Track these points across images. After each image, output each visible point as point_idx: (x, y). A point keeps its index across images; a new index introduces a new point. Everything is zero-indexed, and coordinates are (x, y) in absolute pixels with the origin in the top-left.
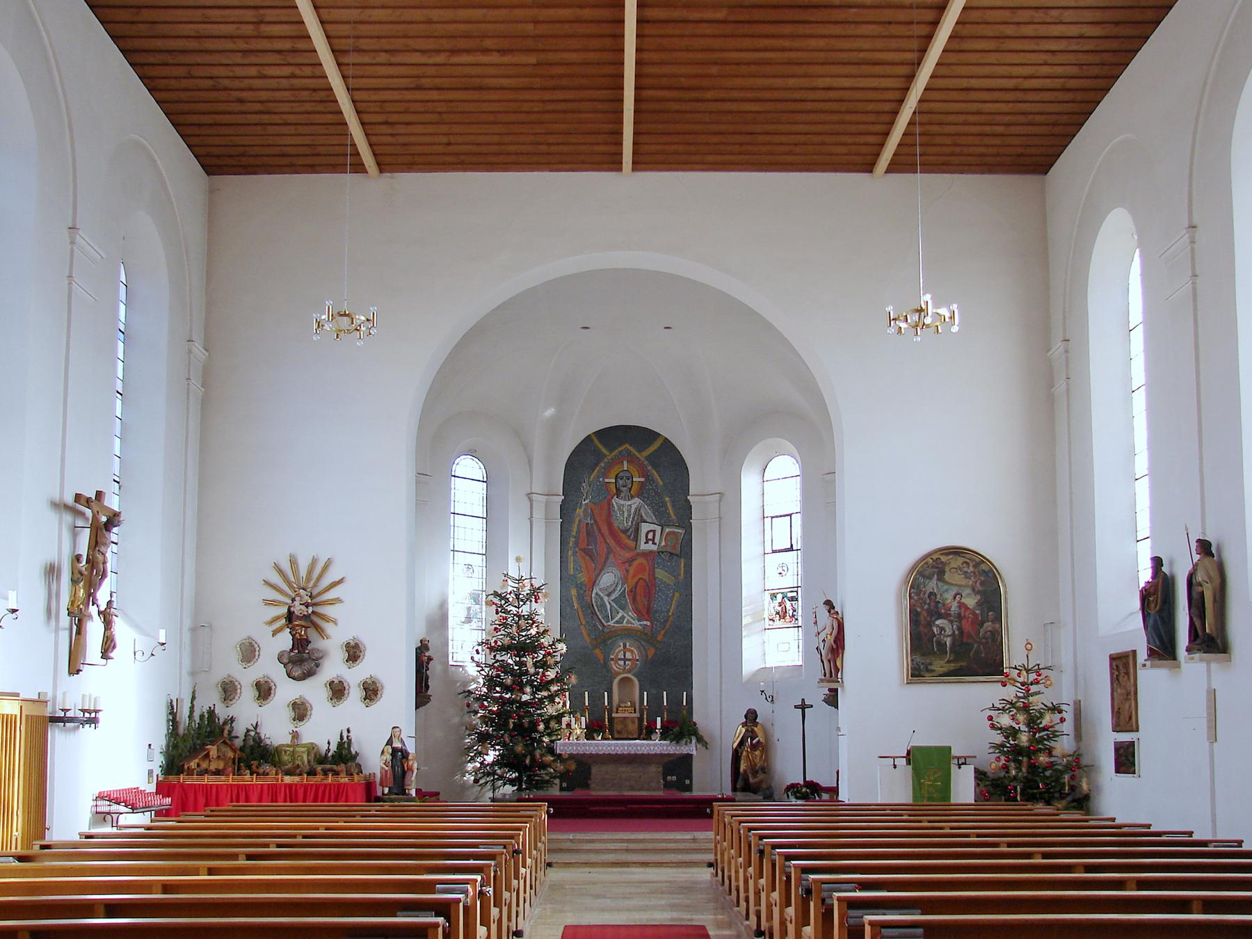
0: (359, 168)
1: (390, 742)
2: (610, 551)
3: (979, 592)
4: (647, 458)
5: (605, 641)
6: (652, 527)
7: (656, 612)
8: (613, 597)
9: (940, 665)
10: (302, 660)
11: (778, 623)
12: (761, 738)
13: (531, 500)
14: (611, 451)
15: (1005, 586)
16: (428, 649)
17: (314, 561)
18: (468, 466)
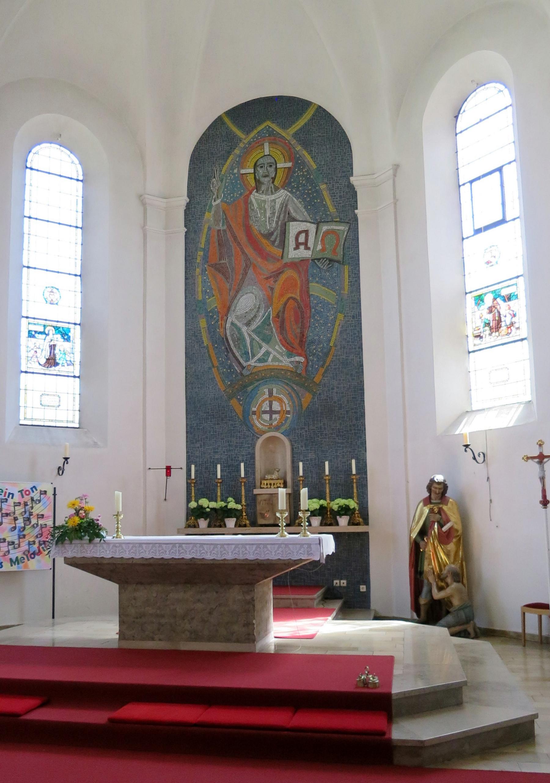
2: (248, 264)
4: (296, 135)
6: (304, 226)
7: (312, 342)
8: (254, 326)
11: (489, 339)
12: (454, 521)
14: (248, 133)
18: (51, 158)
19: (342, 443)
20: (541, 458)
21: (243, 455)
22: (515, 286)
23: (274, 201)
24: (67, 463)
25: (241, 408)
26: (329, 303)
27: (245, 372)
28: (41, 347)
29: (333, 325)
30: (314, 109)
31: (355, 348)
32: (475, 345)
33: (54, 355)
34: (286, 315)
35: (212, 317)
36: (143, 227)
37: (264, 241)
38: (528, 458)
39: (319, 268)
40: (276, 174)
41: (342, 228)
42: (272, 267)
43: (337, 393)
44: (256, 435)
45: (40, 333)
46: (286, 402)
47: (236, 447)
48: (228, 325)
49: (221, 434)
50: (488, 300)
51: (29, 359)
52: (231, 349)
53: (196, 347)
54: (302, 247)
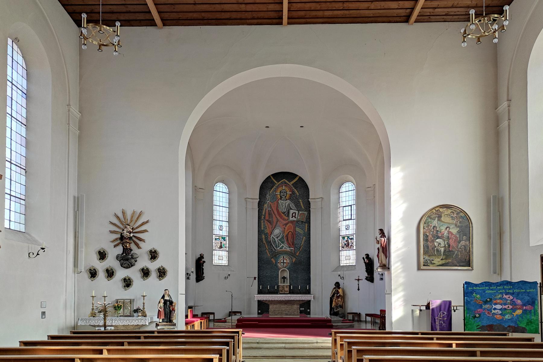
0: (151, 23)
1: (163, 297)
2: (278, 221)
3: (458, 227)
4: (293, 184)
5: (275, 256)
9: (437, 261)
10: (127, 259)
13: (246, 201)
15: (472, 223)
16: (203, 258)
17: (134, 212)
20: (358, 280)
41: (306, 213)
42: (285, 222)
50: (346, 238)
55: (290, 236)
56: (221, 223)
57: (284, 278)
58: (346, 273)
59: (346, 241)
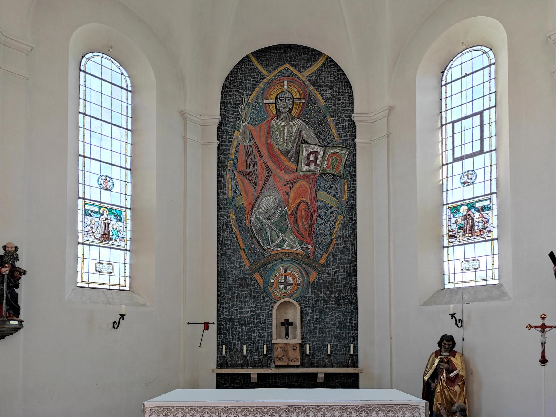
2: (269, 173)
4: (309, 78)
7: (318, 235)
8: (274, 220)
14: (270, 72)
19: (340, 308)
20: (543, 328)
21: (263, 315)
22: (489, 201)
23: (291, 127)
24: (123, 319)
25: (262, 280)
26: (332, 207)
27: (265, 254)
28: (97, 224)
29: (335, 223)
30: (324, 59)
31: (351, 241)
32: (449, 242)
33: (108, 231)
34: (299, 214)
35: (239, 211)
36: (185, 138)
37: (283, 157)
38: (531, 327)
39: (325, 180)
40: (293, 106)
41: (344, 152)
42: (289, 177)
43: (336, 272)
44: (273, 301)
45: (95, 212)
46: (298, 277)
47: (258, 308)
48: (253, 218)
49: (246, 298)
50: (463, 210)
51: (86, 233)
52: (254, 236)
53: (227, 233)
54: (312, 164)
55: (301, 213)
56: (106, 170)
57: (287, 324)
58: (468, 310)
59: (465, 217)
